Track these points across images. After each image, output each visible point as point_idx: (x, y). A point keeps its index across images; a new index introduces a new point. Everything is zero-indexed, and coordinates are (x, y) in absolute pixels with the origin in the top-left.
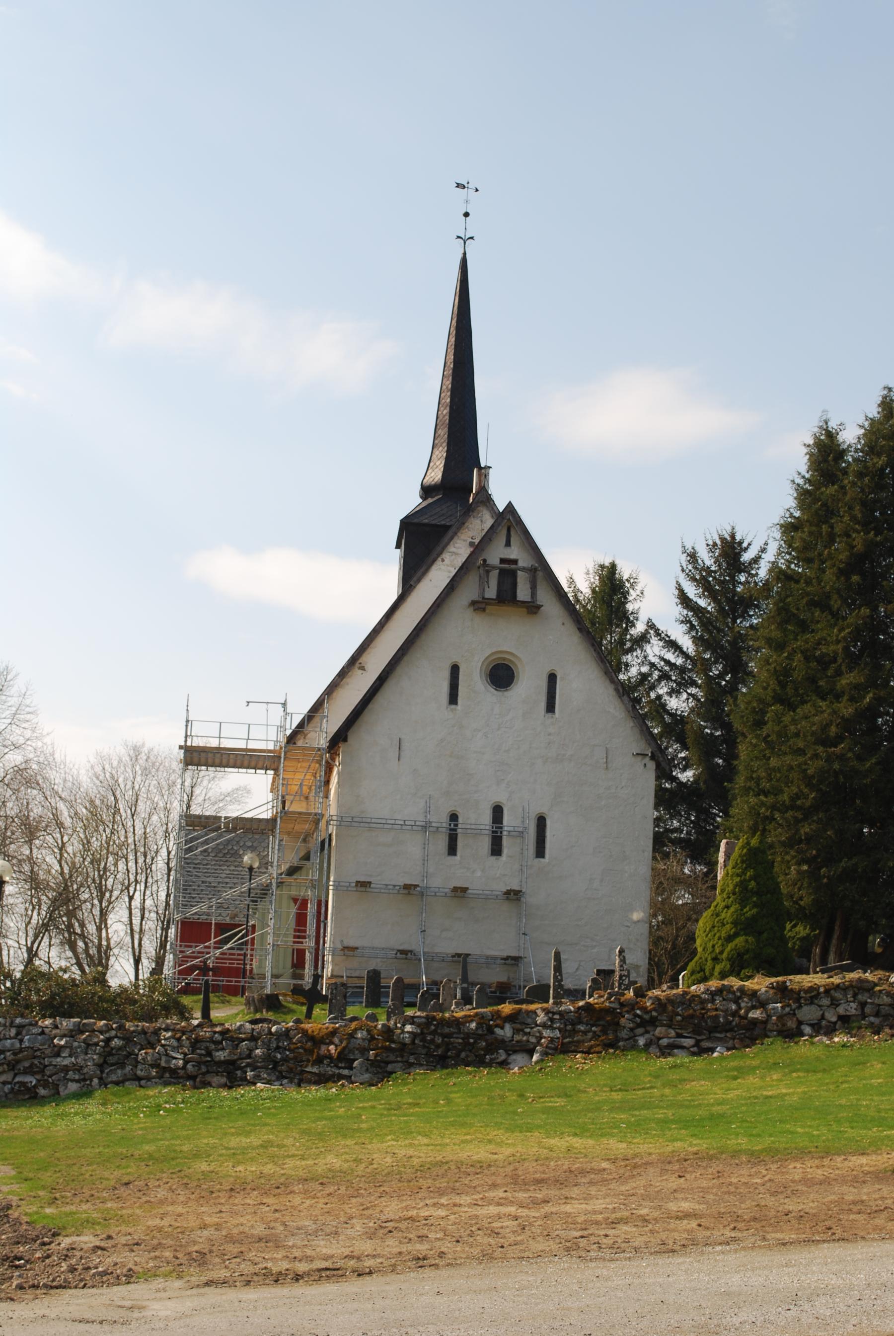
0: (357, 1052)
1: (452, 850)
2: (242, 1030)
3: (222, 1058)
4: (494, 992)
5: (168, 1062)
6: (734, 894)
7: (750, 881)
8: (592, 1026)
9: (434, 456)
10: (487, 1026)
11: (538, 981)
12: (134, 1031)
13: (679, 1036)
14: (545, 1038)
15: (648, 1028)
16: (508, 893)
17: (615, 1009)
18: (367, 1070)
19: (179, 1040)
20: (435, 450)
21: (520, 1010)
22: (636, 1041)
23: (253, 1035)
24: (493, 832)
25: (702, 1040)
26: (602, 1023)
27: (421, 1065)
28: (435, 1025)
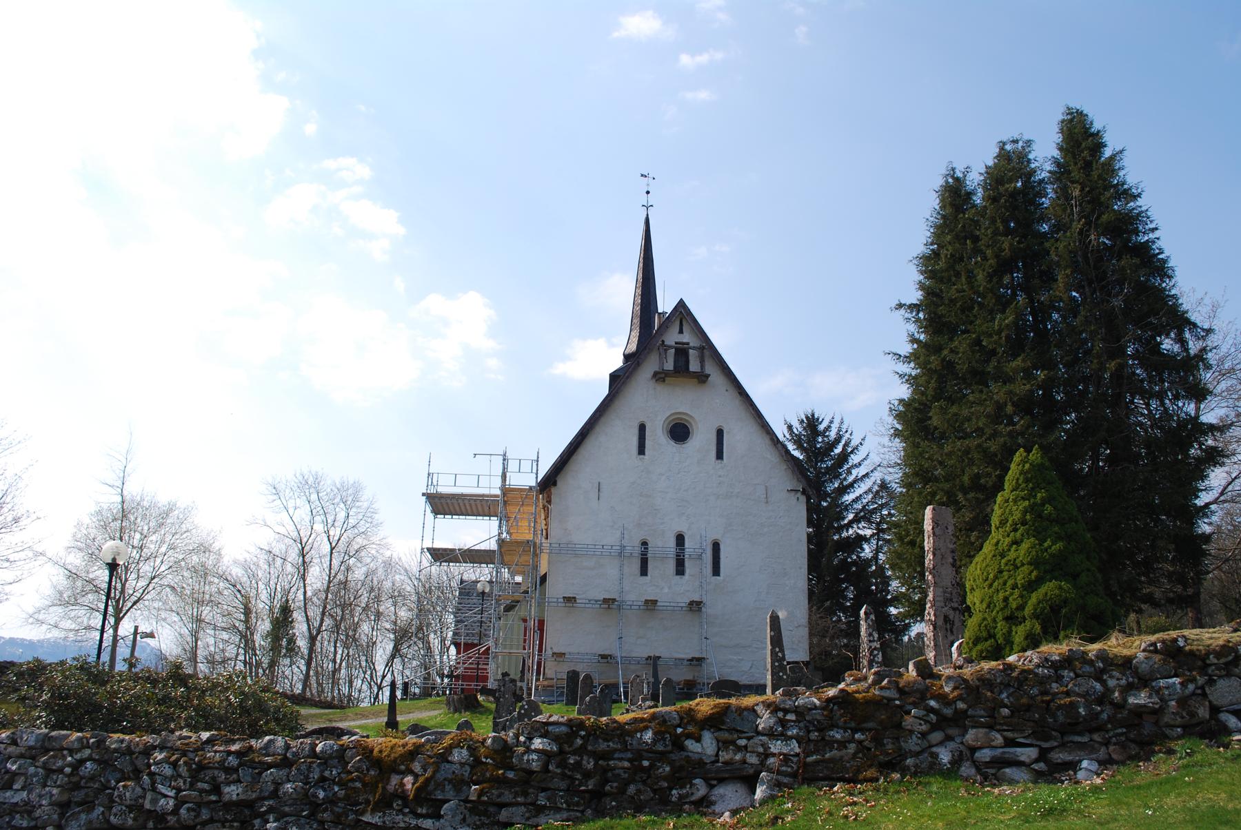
0: (448, 787)
1: (644, 572)
2: (271, 750)
3: (235, 797)
5: (154, 801)
6: (1024, 523)
7: (1043, 505)
8: (855, 731)
10: (673, 735)
12: (116, 750)
13: (1010, 743)
14: (774, 755)
15: (951, 732)
16: (691, 603)
17: (890, 700)
18: (464, 820)
19: (175, 765)
21: (728, 707)
22: (935, 756)
23: (285, 757)
25: (1052, 749)
26: (871, 725)
27: (559, 810)
28: (582, 738)
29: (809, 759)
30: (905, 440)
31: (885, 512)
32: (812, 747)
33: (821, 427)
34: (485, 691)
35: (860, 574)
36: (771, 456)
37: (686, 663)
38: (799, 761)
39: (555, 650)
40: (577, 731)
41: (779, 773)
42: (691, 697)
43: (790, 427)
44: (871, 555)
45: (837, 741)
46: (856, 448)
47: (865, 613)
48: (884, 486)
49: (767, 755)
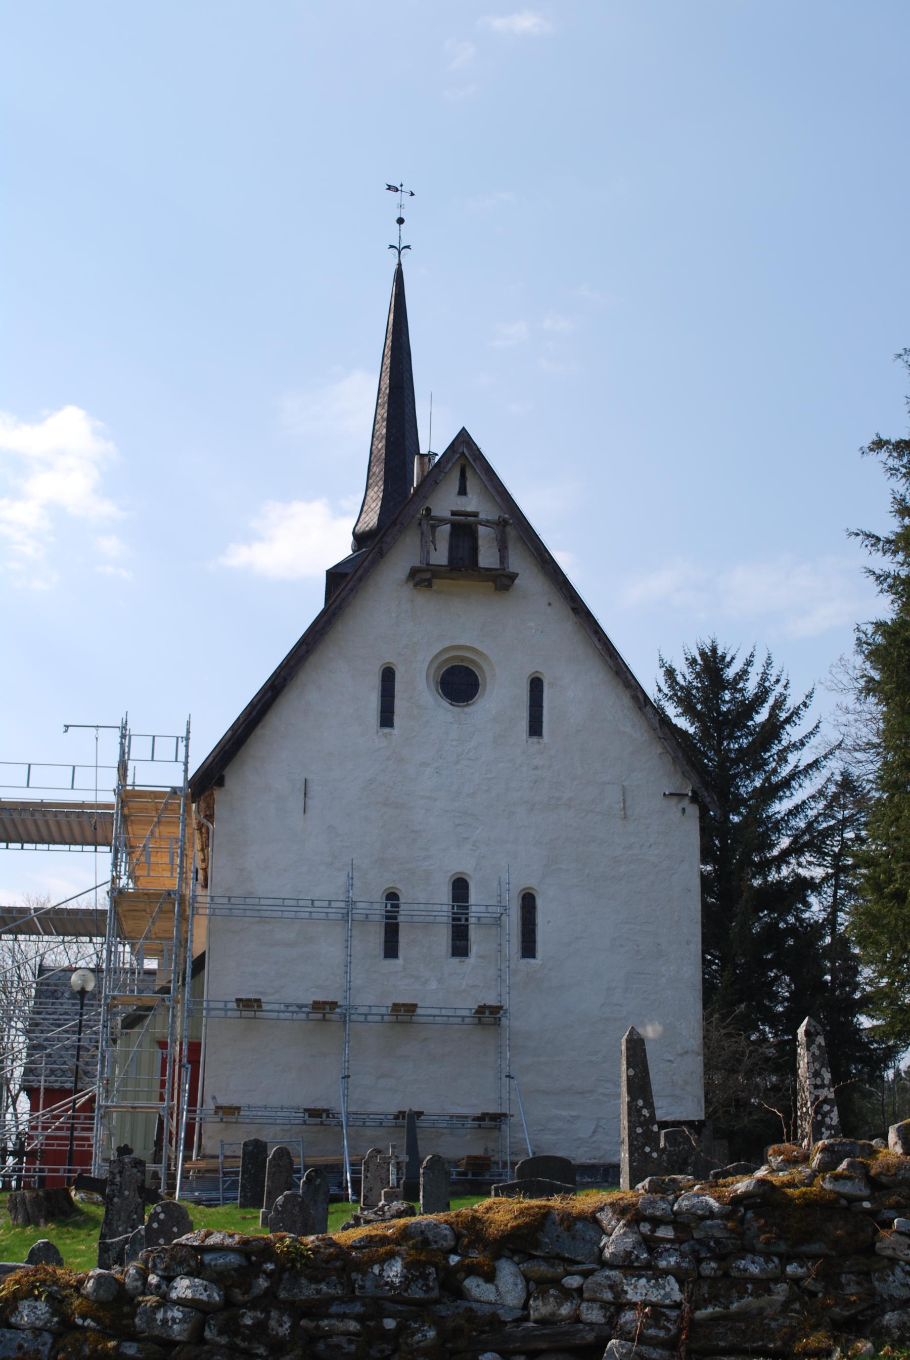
1: (391, 950)
4: (464, 1174)
8: (786, 1259)
9: (368, 498)
11: (534, 1153)
14: (633, 1306)
16: (481, 1010)
17: (853, 1200)
20: (369, 491)
21: (546, 1214)
24: (454, 919)
26: (815, 1248)
28: (269, 1275)
29: (701, 1314)
30: (886, 699)
31: (850, 835)
32: (705, 1290)
33: (730, 673)
34: (86, 1184)
35: (803, 950)
36: (633, 730)
37: (470, 1123)
38: (681, 1317)
39: (223, 1101)
40: (260, 1264)
41: (643, 1340)
42: (481, 1191)
43: (670, 673)
44: (822, 916)
45: (753, 1279)
46: (796, 712)
47: (807, 1033)
48: (847, 784)
49: (620, 1305)
